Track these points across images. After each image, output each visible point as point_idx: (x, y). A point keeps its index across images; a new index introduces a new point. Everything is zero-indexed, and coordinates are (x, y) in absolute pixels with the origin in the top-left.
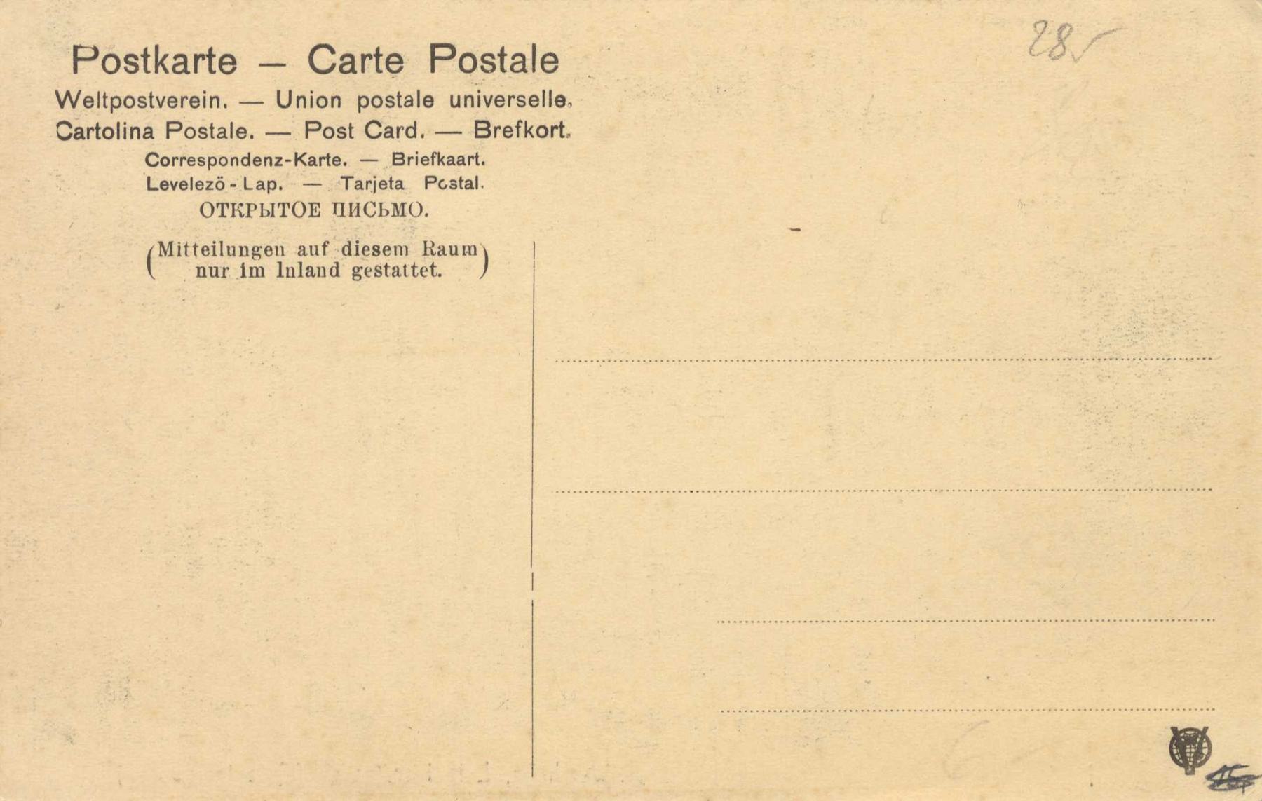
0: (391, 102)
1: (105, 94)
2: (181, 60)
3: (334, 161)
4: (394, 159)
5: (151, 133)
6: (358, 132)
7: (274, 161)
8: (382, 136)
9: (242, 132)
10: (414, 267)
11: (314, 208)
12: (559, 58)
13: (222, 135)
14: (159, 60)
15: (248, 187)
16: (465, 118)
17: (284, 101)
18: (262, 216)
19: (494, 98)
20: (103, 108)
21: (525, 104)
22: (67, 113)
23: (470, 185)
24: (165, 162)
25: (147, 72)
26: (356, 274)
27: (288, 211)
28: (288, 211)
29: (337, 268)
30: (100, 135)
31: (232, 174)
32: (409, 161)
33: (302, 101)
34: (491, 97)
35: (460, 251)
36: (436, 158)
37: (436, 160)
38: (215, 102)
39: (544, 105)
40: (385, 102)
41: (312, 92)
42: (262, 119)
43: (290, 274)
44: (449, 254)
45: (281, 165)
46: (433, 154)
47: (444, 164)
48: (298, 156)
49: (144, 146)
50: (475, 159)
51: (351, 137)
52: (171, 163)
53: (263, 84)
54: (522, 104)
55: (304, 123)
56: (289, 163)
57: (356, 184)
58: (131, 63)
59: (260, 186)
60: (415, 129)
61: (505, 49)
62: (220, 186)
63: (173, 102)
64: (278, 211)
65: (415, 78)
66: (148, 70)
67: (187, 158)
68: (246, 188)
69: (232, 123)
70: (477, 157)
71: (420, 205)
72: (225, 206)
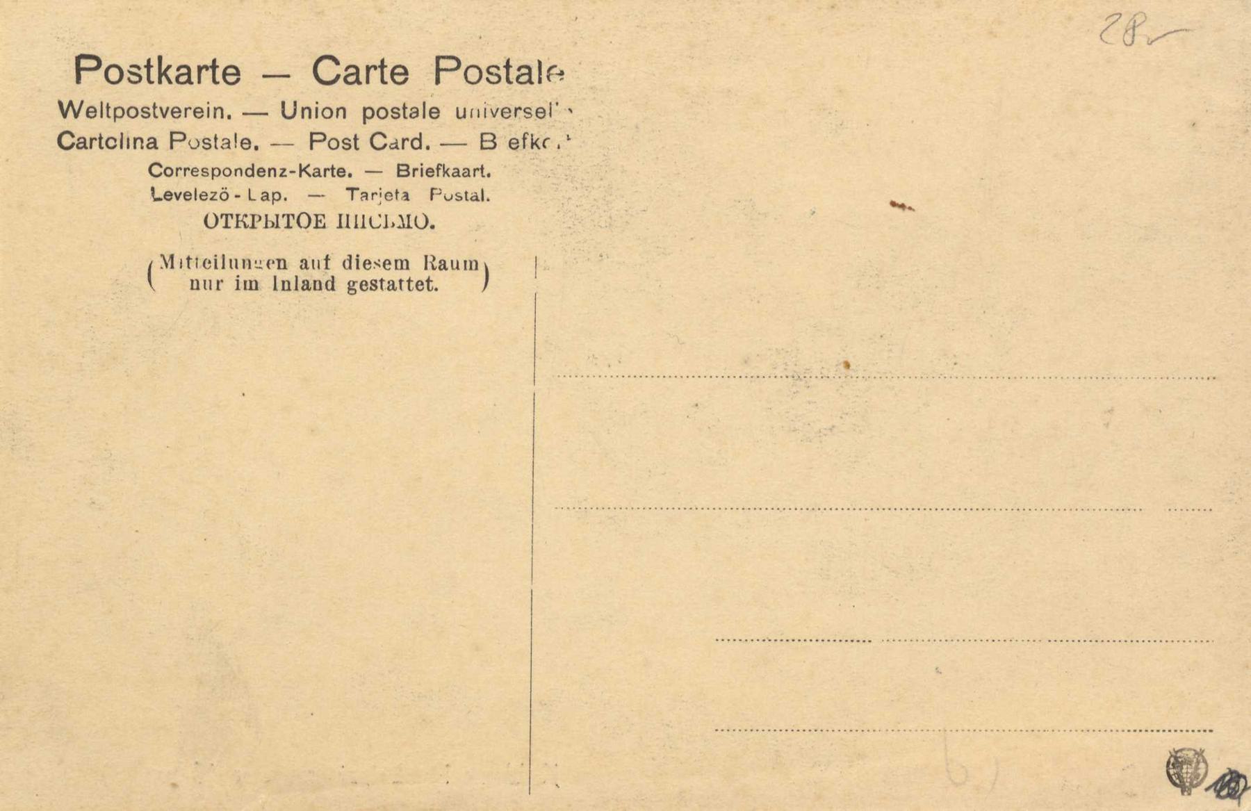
0: (147, 113)
1: (108, 104)
2: (184, 71)
3: (338, 172)
4: (399, 170)
5: (155, 143)
6: (363, 143)
7: (279, 172)
8: (75, 146)
9: (246, 143)
10: (409, 281)
11: (319, 219)
12: (240, 70)
13: (394, 146)
14: (163, 70)
15: (252, 198)
16: (469, 131)
17: (289, 112)
18: (266, 227)
19: (170, 110)
20: (107, 118)
21: (149, 116)
22: (70, 123)
23: (479, 197)
24: (169, 172)
25: (151, 82)
26: (351, 289)
27: (293, 222)
28: (293, 222)
29: (333, 282)
30: (103, 144)
31: (239, 184)
32: (414, 173)
33: (306, 112)
34: (168, 108)
35: (461, 265)
36: (441, 169)
37: (441, 172)
38: (219, 112)
39: (208, 116)
40: (390, 113)
41: (317, 103)
42: (262, 131)
43: (286, 287)
44: (450, 268)
45: (286, 176)
46: (438, 166)
47: (449, 176)
48: (303, 167)
49: (150, 156)
50: (480, 171)
51: (356, 148)
52: (174, 174)
53: (270, 95)
54: (397, 116)
55: (309, 134)
56: (293, 174)
57: (261, 196)
58: (136, 75)
59: (265, 197)
60: (420, 140)
61: (152, 60)
62: (224, 196)
63: (176, 112)
64: (283, 222)
65: (419, 89)
66: (152, 79)
67: (191, 169)
68: (250, 199)
69: (236, 135)
70: (482, 168)
71: (425, 216)
72: (229, 217)
